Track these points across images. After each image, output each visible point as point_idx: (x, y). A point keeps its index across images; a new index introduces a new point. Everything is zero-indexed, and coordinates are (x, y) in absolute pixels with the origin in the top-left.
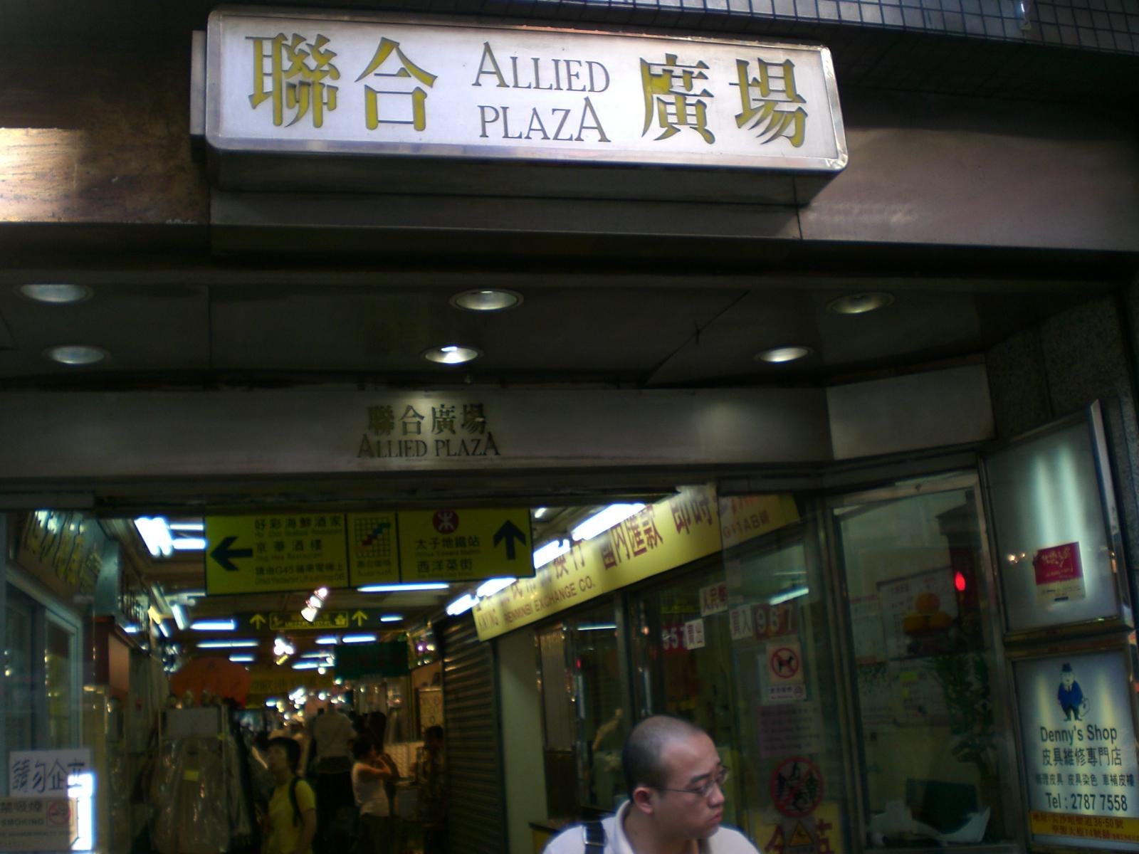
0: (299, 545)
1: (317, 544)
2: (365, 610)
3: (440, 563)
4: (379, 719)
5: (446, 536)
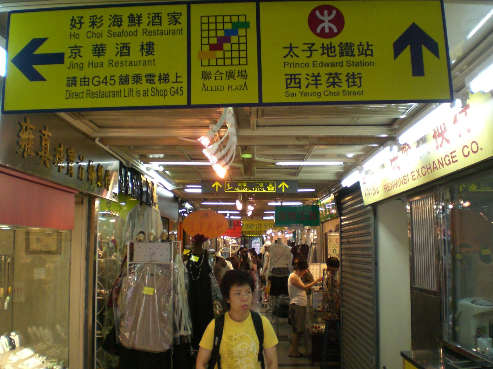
0: (125, 49)
1: (148, 49)
2: (286, 181)
3: (316, 77)
4: (305, 248)
5: (326, 41)
